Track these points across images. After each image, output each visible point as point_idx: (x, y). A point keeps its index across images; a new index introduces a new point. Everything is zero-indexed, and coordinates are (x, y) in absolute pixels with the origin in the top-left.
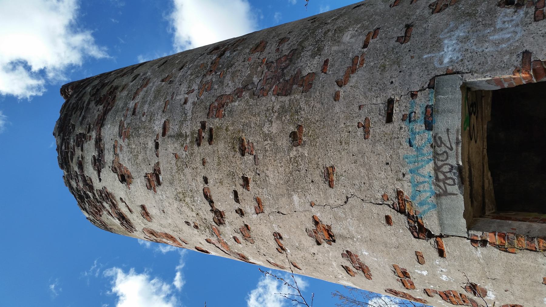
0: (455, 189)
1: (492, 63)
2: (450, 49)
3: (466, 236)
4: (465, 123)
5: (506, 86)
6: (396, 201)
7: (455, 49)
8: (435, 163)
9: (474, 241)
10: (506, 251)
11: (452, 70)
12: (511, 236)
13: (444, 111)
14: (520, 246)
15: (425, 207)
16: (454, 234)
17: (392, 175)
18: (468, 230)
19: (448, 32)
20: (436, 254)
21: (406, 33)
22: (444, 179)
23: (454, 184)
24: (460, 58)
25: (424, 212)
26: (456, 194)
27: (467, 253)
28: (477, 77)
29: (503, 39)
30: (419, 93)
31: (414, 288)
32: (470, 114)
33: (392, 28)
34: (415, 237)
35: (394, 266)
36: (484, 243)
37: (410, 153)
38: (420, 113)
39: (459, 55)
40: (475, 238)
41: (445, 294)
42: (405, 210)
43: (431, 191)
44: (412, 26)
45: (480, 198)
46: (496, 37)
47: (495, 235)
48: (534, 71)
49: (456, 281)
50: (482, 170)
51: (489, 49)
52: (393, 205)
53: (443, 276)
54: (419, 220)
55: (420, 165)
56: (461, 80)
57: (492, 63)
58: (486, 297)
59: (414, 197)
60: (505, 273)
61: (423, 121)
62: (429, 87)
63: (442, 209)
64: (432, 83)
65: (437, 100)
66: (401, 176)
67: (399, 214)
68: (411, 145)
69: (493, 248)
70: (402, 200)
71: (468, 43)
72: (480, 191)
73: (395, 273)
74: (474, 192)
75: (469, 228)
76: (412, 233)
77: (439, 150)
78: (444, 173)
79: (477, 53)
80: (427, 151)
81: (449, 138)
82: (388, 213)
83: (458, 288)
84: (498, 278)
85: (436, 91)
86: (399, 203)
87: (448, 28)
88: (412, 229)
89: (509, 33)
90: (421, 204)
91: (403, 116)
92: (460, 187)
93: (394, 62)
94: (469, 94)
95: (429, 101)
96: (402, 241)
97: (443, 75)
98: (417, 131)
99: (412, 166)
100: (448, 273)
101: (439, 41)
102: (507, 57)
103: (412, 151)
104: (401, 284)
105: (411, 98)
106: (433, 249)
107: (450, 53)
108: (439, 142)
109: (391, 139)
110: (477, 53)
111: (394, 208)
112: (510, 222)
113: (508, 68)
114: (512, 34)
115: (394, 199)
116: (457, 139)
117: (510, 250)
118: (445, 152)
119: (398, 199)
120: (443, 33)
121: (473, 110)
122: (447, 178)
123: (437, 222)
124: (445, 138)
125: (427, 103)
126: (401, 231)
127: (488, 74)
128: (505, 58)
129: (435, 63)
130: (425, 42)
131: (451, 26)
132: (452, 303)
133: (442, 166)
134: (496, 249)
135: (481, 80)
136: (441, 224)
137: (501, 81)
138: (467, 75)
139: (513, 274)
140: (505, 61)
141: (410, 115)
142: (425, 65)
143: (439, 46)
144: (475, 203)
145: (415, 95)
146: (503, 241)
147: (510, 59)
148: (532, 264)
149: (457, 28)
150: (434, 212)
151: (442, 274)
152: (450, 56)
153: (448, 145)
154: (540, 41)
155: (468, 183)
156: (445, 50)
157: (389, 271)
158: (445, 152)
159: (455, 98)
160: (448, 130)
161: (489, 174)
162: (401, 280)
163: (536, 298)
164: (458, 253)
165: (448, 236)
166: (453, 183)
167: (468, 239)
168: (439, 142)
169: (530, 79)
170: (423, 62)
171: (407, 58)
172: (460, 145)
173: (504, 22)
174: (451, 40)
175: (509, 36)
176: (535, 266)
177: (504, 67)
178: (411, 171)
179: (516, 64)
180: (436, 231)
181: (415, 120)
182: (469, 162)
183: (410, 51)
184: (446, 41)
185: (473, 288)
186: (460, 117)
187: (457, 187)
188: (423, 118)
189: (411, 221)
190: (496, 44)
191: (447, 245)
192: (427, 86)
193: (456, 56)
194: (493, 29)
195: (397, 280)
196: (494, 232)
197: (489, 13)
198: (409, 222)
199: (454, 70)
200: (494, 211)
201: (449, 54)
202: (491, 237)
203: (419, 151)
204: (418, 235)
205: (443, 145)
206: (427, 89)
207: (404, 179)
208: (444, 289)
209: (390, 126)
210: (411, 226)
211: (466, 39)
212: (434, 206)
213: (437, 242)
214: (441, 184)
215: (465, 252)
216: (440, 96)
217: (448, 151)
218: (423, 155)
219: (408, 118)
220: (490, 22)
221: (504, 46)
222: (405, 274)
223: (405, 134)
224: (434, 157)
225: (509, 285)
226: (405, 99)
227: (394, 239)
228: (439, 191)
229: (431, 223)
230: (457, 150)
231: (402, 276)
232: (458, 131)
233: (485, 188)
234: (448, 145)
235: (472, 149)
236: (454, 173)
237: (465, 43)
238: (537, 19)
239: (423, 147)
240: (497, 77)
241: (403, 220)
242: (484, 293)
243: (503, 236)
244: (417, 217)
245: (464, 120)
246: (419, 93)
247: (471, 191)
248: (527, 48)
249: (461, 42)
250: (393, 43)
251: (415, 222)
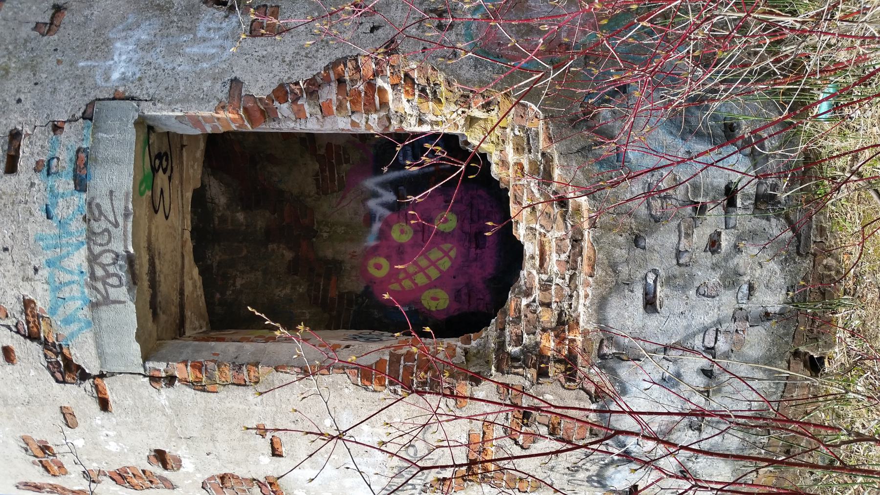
0: (121, 293)
1: (186, 90)
2: (124, 57)
3: (142, 372)
4: (141, 184)
5: (596, 301)
6: (22, 319)
7: (131, 60)
8: (89, 249)
9: (154, 379)
10: (204, 391)
11: (124, 92)
12: (211, 365)
13: (106, 160)
14: (223, 379)
15: (74, 327)
16: (122, 369)
17: (13, 269)
18: (144, 362)
19: (123, 30)
20: (95, 406)
21: (53, 17)
22: (103, 276)
23: (121, 285)
24: (138, 76)
25: (72, 335)
26: (124, 302)
27: (145, 400)
28: (161, 109)
29: (205, 54)
30: (66, 126)
31: (66, 473)
32: (154, 170)
33: (29, 5)
34: (57, 381)
35: (25, 440)
36: (171, 380)
37: (48, 231)
38: (67, 159)
39: (137, 70)
40: (156, 374)
41: (120, 475)
42: (39, 333)
43: (83, 299)
44: (66, 9)
45: (174, 309)
46: (195, 50)
47: (186, 366)
48: (246, 110)
49: (132, 450)
50: (180, 263)
51: (184, 67)
52: (16, 326)
53: (110, 443)
54: (65, 351)
55: (64, 252)
56: (137, 110)
57: (186, 90)
58: (182, 469)
59: (53, 310)
60: (204, 426)
61: (71, 174)
62: (84, 117)
63: (100, 328)
64: (89, 111)
65: (96, 141)
66: (31, 272)
67: (28, 341)
68: (49, 217)
69: (184, 387)
70: (33, 316)
71: (152, 53)
72: (175, 298)
73: (26, 450)
74: (159, 299)
75: (146, 358)
76: (53, 375)
77: (97, 227)
78: (104, 266)
79: (164, 70)
80: (77, 226)
81: (113, 206)
82: (8, 342)
83: (140, 461)
84: (194, 435)
85: (94, 124)
86: (28, 322)
87: (125, 24)
88: (52, 368)
89: (214, 47)
90: (67, 321)
91: (37, 163)
92: (129, 290)
93: (26, 65)
94: (153, 137)
95: (83, 140)
96: (36, 390)
97: (109, 99)
98: (61, 191)
99: (50, 254)
100: (119, 438)
101: (108, 42)
102: (209, 83)
103: (50, 226)
104: (41, 469)
105: (52, 133)
106: (89, 399)
107: (122, 64)
108: (97, 213)
109: (13, 203)
110: (164, 70)
111: (18, 332)
112: (213, 343)
113: (209, 102)
114: (219, 50)
115: (18, 315)
116: (126, 208)
117: (209, 388)
118: (107, 230)
119: (27, 315)
120: (115, 30)
121: (161, 163)
122: (109, 275)
123: (93, 351)
124: (106, 205)
125: (80, 144)
126: (33, 373)
127: (179, 105)
128: (205, 84)
129: (97, 77)
130: (83, 40)
131: (130, 21)
132: (133, 487)
133: (101, 253)
134: (188, 390)
135: (166, 114)
136: (101, 355)
137: (199, 121)
138: (146, 103)
139: (216, 425)
140: (205, 89)
141: (49, 161)
142: (80, 79)
143: (106, 50)
144: (163, 317)
145: (60, 128)
146: (199, 375)
147: (212, 88)
148: (241, 407)
149: (138, 26)
150: (88, 335)
151: (112, 440)
152: (123, 70)
153: (112, 219)
154: (255, 67)
155: (146, 284)
156: (116, 58)
157: (15, 448)
158: (107, 230)
159: (124, 139)
160: (111, 192)
161: (196, 271)
162: (41, 462)
163: (249, 459)
164: (130, 402)
165: (113, 374)
166: (118, 283)
167: (145, 376)
168: (97, 213)
169: (241, 122)
170: (77, 72)
171: (51, 62)
172: (131, 219)
173: (209, 29)
174: (127, 44)
175: (214, 51)
176: (245, 410)
177: (203, 99)
178: (49, 264)
179: (221, 96)
180: (92, 367)
181: (57, 173)
182: (150, 249)
183: (56, 50)
184: (118, 45)
185: (160, 456)
186: (132, 171)
187: (124, 289)
188: (71, 170)
189: (49, 353)
190: (196, 61)
191: (112, 389)
192: (80, 114)
193: (131, 71)
194: (192, 36)
195: (34, 463)
196: (185, 362)
197: (190, 11)
198: (46, 356)
199: (127, 94)
200: (204, 329)
201: (120, 66)
202: (180, 371)
203: (64, 227)
204: (63, 378)
205: (103, 218)
206: (81, 120)
207: (37, 277)
208: (115, 467)
209: (12, 179)
210: (51, 362)
211: (150, 45)
212: (89, 324)
213: (96, 387)
214: (100, 285)
215: (141, 398)
216: (100, 135)
217: (110, 229)
218: (70, 234)
219: (45, 168)
220: (189, 26)
221: (205, 65)
222: (45, 448)
223: (39, 196)
224: (88, 238)
225: (211, 444)
226: (43, 134)
227: (20, 389)
228: (96, 297)
229: (84, 355)
230: (125, 227)
231: (39, 453)
232: (127, 194)
233: (186, 294)
234: (112, 219)
235: (157, 227)
236: (121, 266)
237: (148, 52)
238: (254, 33)
239: (71, 220)
240: (191, 113)
241: (35, 353)
242: (178, 463)
243: (198, 367)
244: (60, 345)
245: (139, 178)
246: (66, 124)
247: (154, 296)
248: (237, 74)
249: (142, 49)
250: (26, 31)
251: (57, 354)
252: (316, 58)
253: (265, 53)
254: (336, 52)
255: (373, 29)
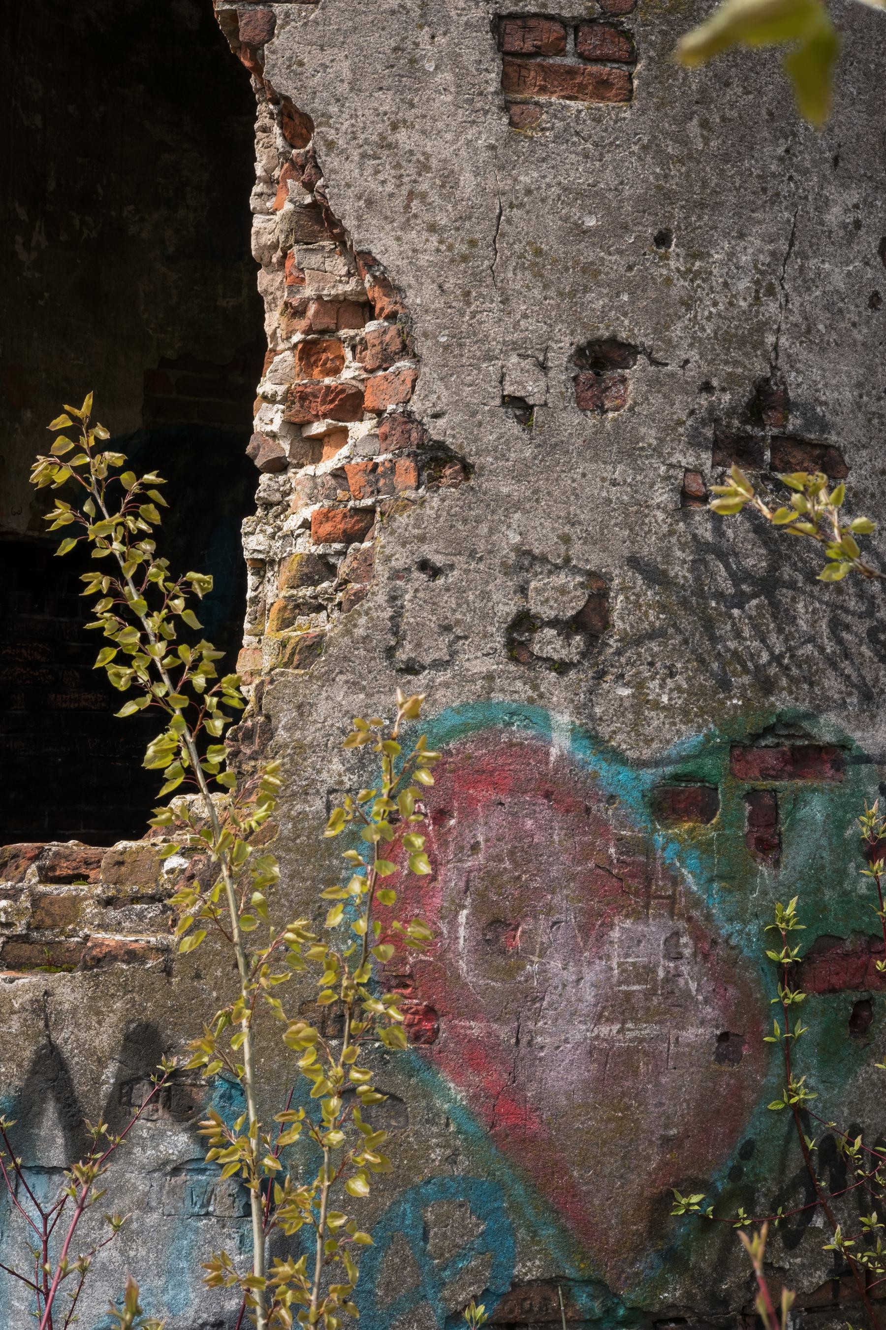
252: (406, 226)
253: (430, 67)
254: (430, 289)
255: (519, 407)
